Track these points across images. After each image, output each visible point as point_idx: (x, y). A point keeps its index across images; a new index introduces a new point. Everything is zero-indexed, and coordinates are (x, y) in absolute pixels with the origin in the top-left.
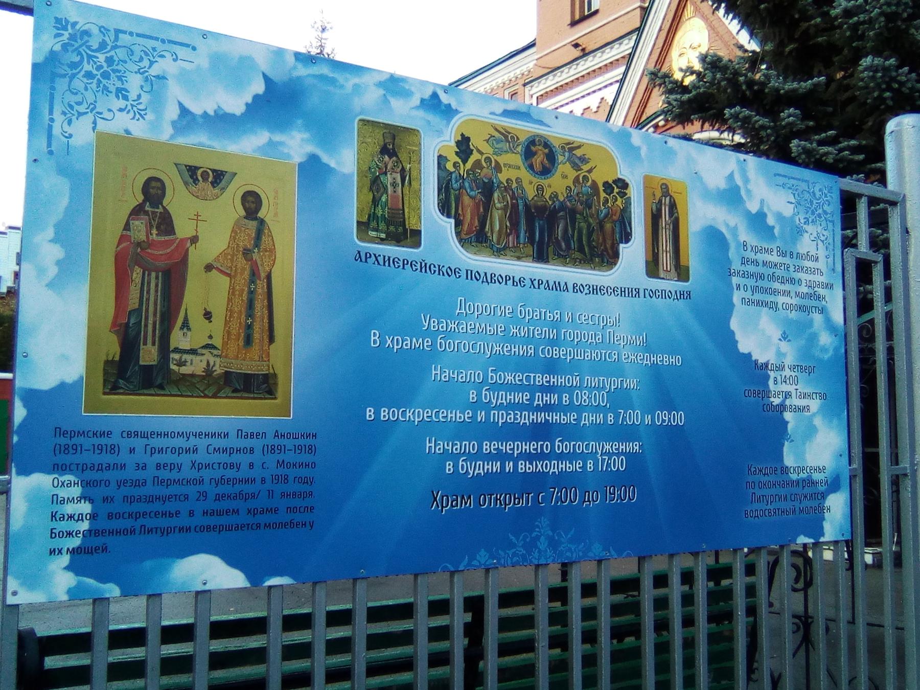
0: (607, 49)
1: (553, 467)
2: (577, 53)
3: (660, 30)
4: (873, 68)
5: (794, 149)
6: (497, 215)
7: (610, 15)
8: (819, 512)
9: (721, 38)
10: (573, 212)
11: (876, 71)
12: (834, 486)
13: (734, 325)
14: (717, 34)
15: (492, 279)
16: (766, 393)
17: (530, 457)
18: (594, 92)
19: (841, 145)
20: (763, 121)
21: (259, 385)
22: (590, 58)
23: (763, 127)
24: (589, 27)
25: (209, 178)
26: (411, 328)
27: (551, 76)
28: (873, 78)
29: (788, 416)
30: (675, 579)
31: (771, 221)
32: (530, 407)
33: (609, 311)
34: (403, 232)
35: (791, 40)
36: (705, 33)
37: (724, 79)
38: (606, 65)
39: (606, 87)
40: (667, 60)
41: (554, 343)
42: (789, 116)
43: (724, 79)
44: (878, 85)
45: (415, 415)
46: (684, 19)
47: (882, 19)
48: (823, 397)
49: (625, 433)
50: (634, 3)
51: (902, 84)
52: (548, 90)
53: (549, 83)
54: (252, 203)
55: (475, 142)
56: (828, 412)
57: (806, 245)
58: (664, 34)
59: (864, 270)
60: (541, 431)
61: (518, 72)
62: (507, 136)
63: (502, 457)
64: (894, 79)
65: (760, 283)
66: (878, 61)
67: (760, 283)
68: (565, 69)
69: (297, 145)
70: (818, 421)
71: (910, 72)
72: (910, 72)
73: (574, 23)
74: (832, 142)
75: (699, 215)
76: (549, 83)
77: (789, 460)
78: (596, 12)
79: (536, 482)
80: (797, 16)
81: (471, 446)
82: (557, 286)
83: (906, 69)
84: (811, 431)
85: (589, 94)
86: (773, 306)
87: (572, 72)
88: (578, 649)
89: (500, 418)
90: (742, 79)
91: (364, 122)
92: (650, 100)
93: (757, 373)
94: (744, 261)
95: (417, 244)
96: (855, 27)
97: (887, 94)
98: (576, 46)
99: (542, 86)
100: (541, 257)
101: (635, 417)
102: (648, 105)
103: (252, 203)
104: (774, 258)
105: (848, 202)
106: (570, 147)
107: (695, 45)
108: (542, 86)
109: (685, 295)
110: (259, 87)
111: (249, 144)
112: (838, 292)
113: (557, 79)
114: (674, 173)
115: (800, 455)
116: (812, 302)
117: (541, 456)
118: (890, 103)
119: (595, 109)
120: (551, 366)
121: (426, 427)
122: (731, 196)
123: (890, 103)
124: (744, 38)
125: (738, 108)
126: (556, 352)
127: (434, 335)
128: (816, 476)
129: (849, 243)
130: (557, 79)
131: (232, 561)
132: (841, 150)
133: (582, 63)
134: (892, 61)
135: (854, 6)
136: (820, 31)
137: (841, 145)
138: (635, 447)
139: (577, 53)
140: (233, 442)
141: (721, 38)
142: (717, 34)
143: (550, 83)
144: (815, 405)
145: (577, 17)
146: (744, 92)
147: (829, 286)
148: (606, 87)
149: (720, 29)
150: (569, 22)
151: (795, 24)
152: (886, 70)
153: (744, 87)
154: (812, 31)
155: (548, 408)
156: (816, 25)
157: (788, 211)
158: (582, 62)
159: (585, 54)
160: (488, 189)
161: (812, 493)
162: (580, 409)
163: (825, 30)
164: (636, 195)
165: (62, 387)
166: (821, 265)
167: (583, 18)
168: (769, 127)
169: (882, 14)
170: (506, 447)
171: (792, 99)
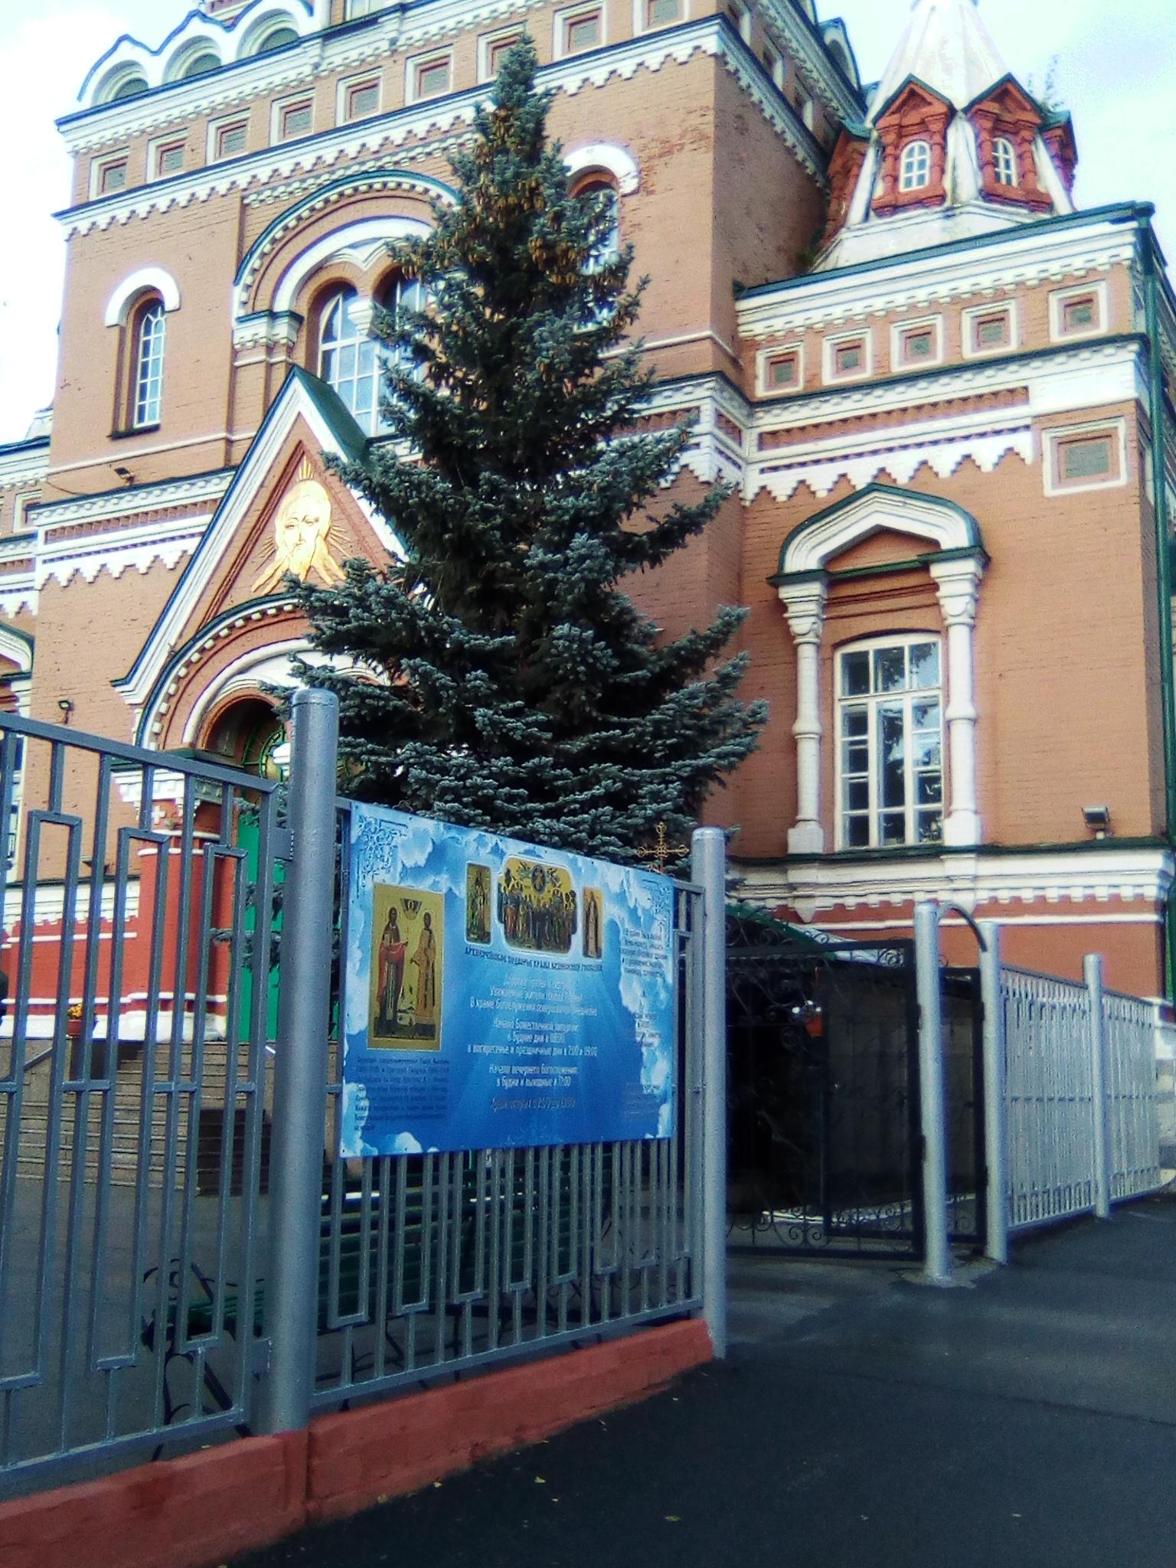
0: (171, 488)
1: (541, 1083)
2: (120, 481)
3: (262, 486)
6: (521, 920)
7: (176, 439)
8: (656, 1116)
9: (349, 518)
10: (552, 916)
11: (572, 641)
12: (664, 1101)
13: (621, 987)
14: (343, 511)
15: (520, 962)
16: (633, 1034)
17: (532, 1077)
18: (144, 544)
19: (530, 719)
20: (446, 679)
21: (426, 1031)
22: (142, 494)
23: (444, 687)
24: (142, 447)
25: (411, 905)
26: (486, 997)
27: (73, 507)
28: (568, 649)
29: (644, 1049)
30: (496, 1189)
31: (640, 912)
32: (531, 1044)
33: (562, 976)
34: (484, 936)
35: (474, 578)
38: (166, 510)
39: (163, 540)
40: (267, 529)
41: (543, 1002)
42: (476, 679)
44: (572, 657)
45: (487, 1049)
46: (296, 478)
47: (583, 585)
48: (660, 1036)
49: (570, 1061)
50: (215, 431)
53: (69, 515)
54: (427, 918)
55: (513, 873)
56: (664, 1044)
57: (656, 929)
58: (266, 494)
59: (682, 943)
60: (536, 1060)
62: (525, 867)
63: (519, 1076)
64: (589, 653)
65: (634, 957)
66: (576, 631)
67: (634, 957)
68: (100, 502)
69: (444, 881)
70: (657, 1053)
72: (606, 648)
74: (516, 713)
75: (609, 911)
76: (69, 515)
77: (643, 1082)
78: (155, 429)
79: (533, 1092)
81: (506, 1069)
82: (545, 966)
83: (603, 643)
84: (654, 1061)
85: (135, 546)
86: (639, 974)
87: (110, 507)
88: (530, 1209)
89: (520, 1051)
91: (470, 865)
92: (239, 579)
93: (629, 1018)
94: (628, 942)
95: (488, 942)
99: (55, 518)
100: (539, 947)
101: (576, 1050)
102: (235, 585)
103: (427, 918)
104: (640, 939)
105: (677, 892)
106: (552, 871)
107: (311, 518)
108: (55, 518)
109: (600, 968)
110: (430, 849)
111: (424, 885)
112: (670, 962)
113: (83, 512)
114: (595, 885)
115: (649, 1079)
116: (657, 971)
117: (532, 1077)
118: (583, 678)
119: (143, 570)
120: (542, 1018)
121: (491, 1058)
122: (621, 897)
125: (418, 660)
126: (544, 1009)
127: (494, 998)
128: (656, 1092)
129: (676, 925)
130: (83, 512)
131: (417, 1138)
132: (528, 725)
133: (129, 498)
135: (551, 561)
136: (509, 576)
137: (530, 719)
138: (573, 1071)
139: (120, 481)
140: (418, 1066)
141: (349, 518)
142: (343, 511)
143: (70, 515)
144: (656, 1041)
145: (122, 428)
146: (421, 639)
147: (665, 957)
148: (163, 540)
149: (348, 506)
150: (109, 431)
151: (483, 561)
152: (582, 641)
154: (499, 574)
155: (539, 1045)
156: (504, 568)
157: (647, 905)
158: (127, 496)
160: (517, 902)
161: (653, 1103)
162: (552, 1045)
163: (513, 574)
164: (579, 900)
165: (360, 1033)
166: (662, 942)
167: (131, 433)
169: (583, 579)
170: (521, 1070)
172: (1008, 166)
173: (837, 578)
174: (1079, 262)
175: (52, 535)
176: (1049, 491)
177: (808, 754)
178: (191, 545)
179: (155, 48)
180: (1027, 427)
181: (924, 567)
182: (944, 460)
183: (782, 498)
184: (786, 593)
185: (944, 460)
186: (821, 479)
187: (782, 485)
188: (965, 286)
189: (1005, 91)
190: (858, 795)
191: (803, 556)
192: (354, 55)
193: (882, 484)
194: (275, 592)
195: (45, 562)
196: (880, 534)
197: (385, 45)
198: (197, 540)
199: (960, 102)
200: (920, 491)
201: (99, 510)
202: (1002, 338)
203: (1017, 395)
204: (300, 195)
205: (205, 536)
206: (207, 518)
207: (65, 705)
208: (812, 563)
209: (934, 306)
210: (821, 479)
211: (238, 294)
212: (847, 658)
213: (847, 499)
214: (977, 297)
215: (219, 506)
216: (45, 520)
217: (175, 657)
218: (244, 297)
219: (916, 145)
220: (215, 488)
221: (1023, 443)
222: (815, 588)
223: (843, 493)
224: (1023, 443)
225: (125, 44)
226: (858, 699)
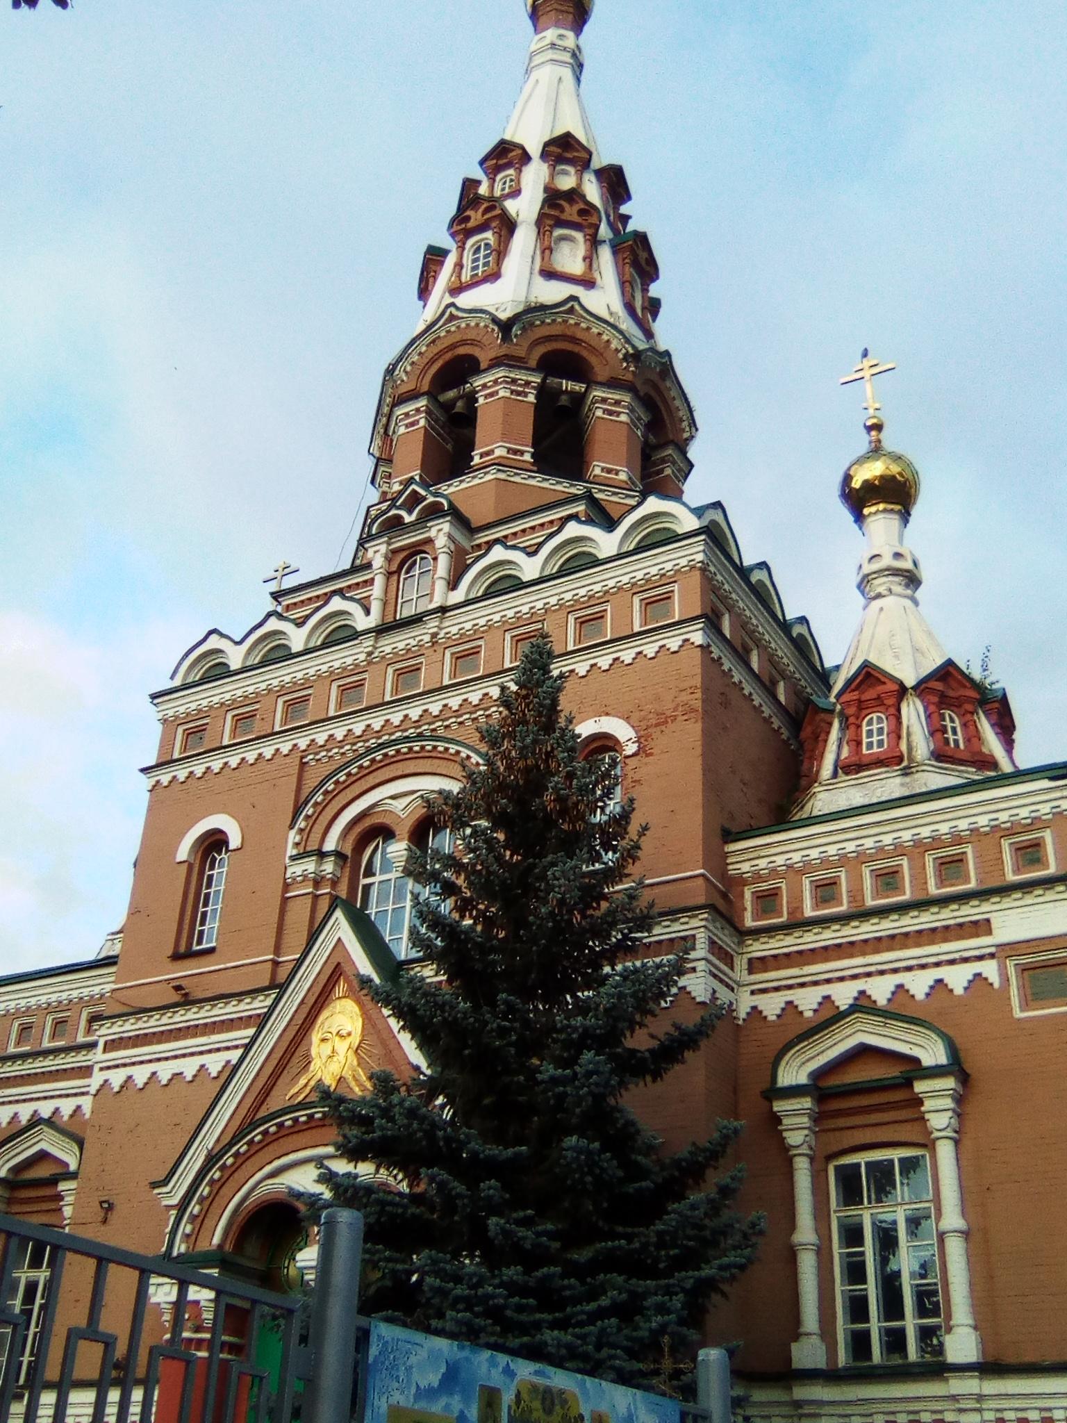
2: (176, 997)
3: (302, 1002)
4: (579, 1151)
5: (492, 1227)
14: (374, 1026)
23: (459, 1196)
28: (577, 1158)
36: (359, 1023)
37: (420, 1130)
42: (490, 1188)
43: (420, 1130)
47: (590, 1099)
51: (603, 1170)
52: (125, 1035)
58: (306, 1009)
61: (75, 994)
71: (612, 1159)
72: (612, 1159)
73: (177, 957)
74: (526, 1222)
78: (211, 951)
80: (499, 1069)
90: (441, 1134)
96: (562, 1097)
97: (589, 1179)
98: (178, 988)
99: (116, 1029)
102: (273, 1093)
107: (344, 1032)
119: (189, 1078)
123: (590, 1187)
124: (416, 1057)
130: (140, 1024)
132: (538, 1234)
134: (597, 1145)
142: (374, 1026)
143: (129, 1027)
145: (182, 949)
150: (170, 953)
152: (590, 1153)
153: (441, 1143)
159: (187, 1001)
167: (190, 955)
168: (466, 1197)
171: (492, 1168)
172: (955, 732)
173: (824, 1090)
174: (1024, 813)
175: (111, 1046)
176: (1018, 1014)
177: (807, 1264)
178: (234, 1056)
179: (238, 639)
180: (992, 956)
181: (908, 1084)
182: (919, 984)
183: (959, 991)
184: (779, 1106)
185: (919, 984)
186: (808, 1000)
187: (771, 1006)
188: (925, 832)
189: (948, 672)
190: (858, 1308)
191: (794, 1072)
192: (401, 645)
193: (863, 1005)
194: (308, 1100)
195: (101, 1069)
196: (863, 1052)
197: (427, 638)
198: (240, 1051)
199: (910, 681)
200: (899, 1011)
201: (154, 1023)
202: (898, 889)
203: (982, 927)
204: (350, 755)
205: (248, 1047)
206: (251, 1032)
207: (106, 1205)
208: (802, 1079)
209: (900, 849)
210: (808, 1000)
211: (293, 836)
212: (837, 1168)
213: (830, 1018)
214: (936, 842)
215: (261, 1021)
216: (106, 1031)
217: (212, 1160)
218: (298, 839)
219: (874, 716)
220: (260, 1004)
221: (990, 969)
222: (807, 1103)
223: (827, 1013)
224: (990, 969)
225: (214, 637)
226: (852, 1211)
